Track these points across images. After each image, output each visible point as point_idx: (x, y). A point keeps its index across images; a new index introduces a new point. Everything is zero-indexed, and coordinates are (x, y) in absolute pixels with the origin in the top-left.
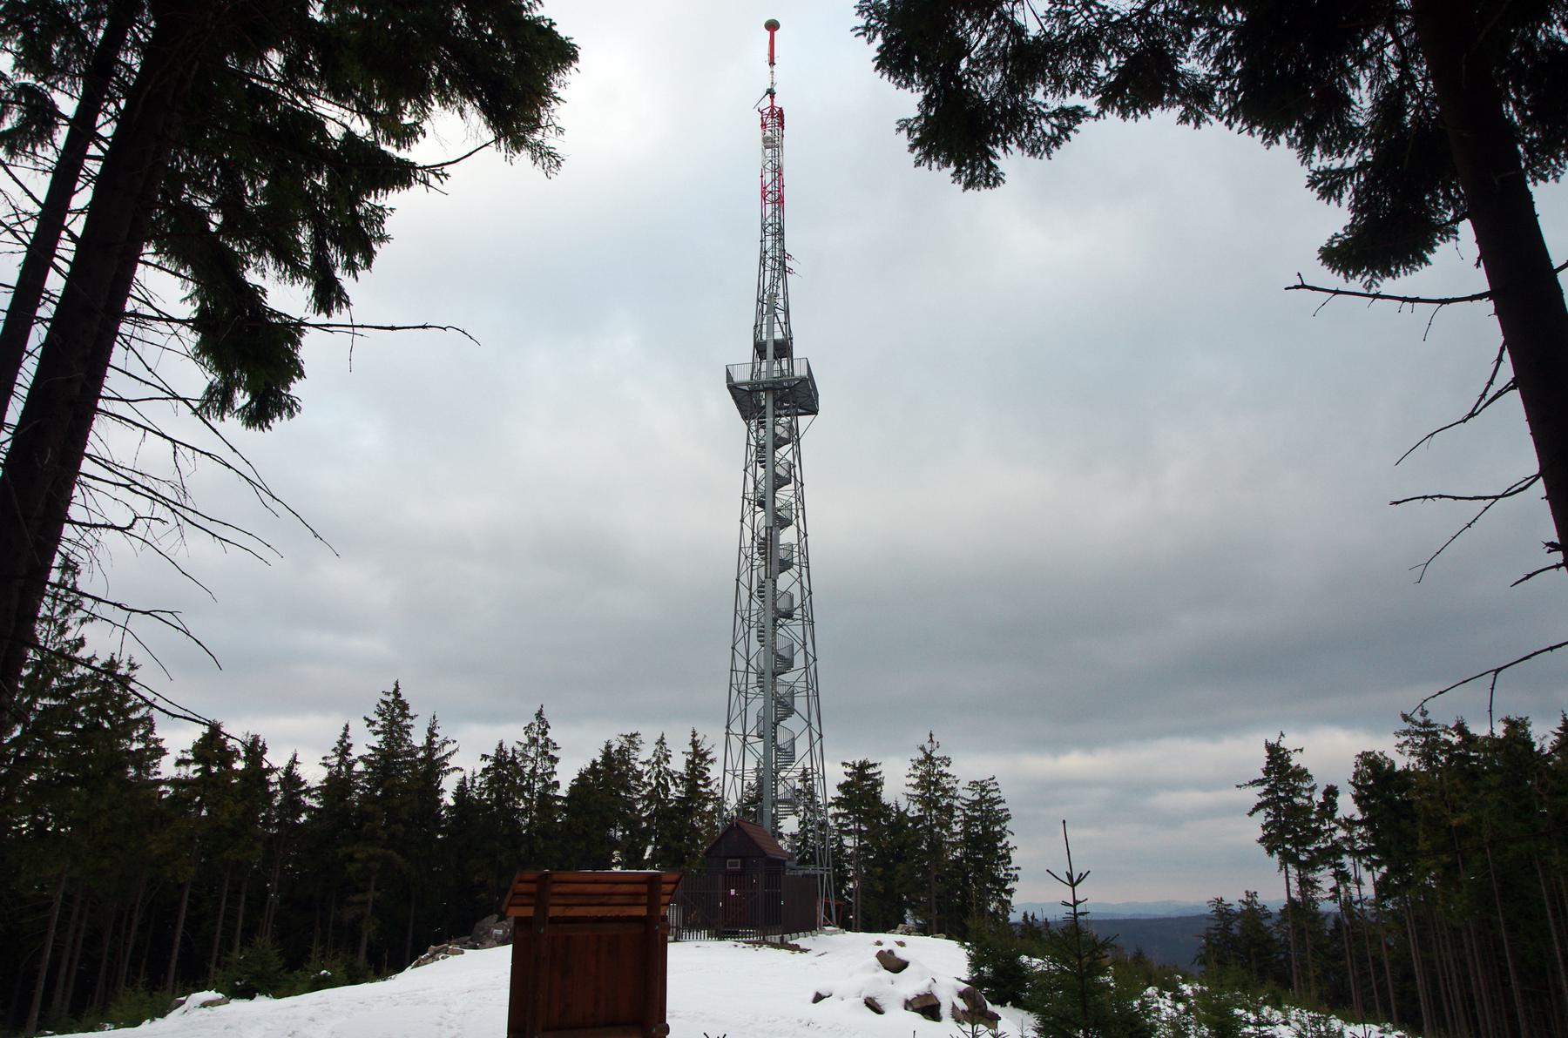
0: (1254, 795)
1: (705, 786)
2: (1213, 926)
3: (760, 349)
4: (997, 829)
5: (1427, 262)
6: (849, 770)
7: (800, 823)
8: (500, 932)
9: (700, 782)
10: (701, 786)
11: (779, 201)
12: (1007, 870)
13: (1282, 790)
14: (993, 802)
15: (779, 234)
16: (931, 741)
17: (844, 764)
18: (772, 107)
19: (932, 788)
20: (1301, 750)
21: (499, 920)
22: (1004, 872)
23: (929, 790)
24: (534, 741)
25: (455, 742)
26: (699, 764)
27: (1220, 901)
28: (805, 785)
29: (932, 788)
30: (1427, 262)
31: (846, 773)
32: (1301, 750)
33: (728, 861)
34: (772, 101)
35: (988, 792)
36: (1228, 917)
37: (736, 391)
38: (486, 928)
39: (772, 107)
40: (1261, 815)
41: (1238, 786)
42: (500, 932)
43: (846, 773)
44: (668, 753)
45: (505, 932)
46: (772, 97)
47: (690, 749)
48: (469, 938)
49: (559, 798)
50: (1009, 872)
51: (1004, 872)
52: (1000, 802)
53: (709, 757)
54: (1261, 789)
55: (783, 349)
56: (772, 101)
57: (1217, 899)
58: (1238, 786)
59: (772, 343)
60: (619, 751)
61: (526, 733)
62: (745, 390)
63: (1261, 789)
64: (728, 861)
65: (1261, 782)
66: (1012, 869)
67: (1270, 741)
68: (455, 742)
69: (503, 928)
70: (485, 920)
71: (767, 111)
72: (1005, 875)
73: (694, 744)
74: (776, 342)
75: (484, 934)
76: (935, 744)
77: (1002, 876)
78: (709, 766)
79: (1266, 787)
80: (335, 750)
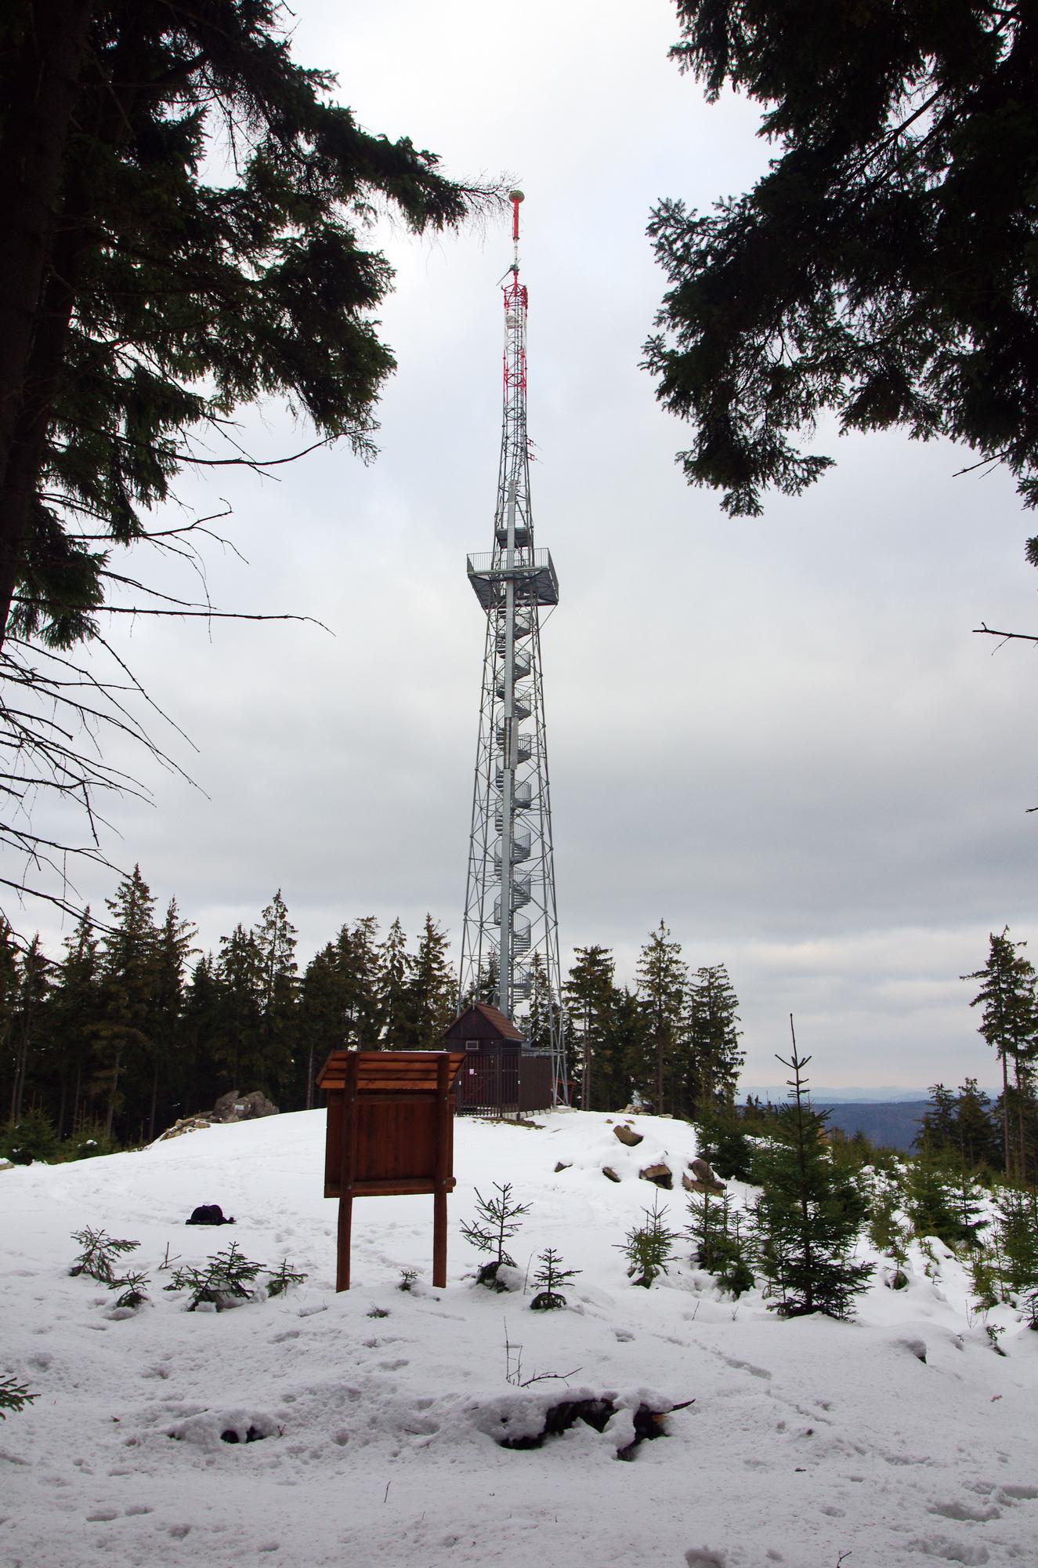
0: (978, 986)
1: (439, 969)
4: (725, 1014)
6: (581, 955)
7: (531, 1006)
8: (242, 1107)
9: (435, 965)
11: (522, 384)
12: (733, 1054)
13: (1004, 982)
15: (522, 418)
19: (662, 974)
20: (1025, 944)
21: (240, 1096)
23: (659, 976)
25: (194, 924)
28: (537, 970)
29: (662, 974)
31: (578, 959)
32: (1025, 944)
34: (516, 278)
35: (717, 979)
40: (984, 1003)
42: (242, 1107)
43: (578, 959)
44: (403, 937)
45: (246, 1107)
46: (516, 274)
47: (426, 934)
48: (211, 1113)
50: (735, 1056)
52: (728, 988)
53: (443, 941)
54: (985, 980)
55: (524, 538)
59: (513, 532)
61: (264, 916)
63: (985, 980)
65: (985, 974)
67: (995, 935)
68: (194, 924)
71: (510, 289)
72: (731, 1059)
73: (429, 928)
74: (517, 531)
77: (728, 1060)
79: (989, 978)
80: (76, 931)
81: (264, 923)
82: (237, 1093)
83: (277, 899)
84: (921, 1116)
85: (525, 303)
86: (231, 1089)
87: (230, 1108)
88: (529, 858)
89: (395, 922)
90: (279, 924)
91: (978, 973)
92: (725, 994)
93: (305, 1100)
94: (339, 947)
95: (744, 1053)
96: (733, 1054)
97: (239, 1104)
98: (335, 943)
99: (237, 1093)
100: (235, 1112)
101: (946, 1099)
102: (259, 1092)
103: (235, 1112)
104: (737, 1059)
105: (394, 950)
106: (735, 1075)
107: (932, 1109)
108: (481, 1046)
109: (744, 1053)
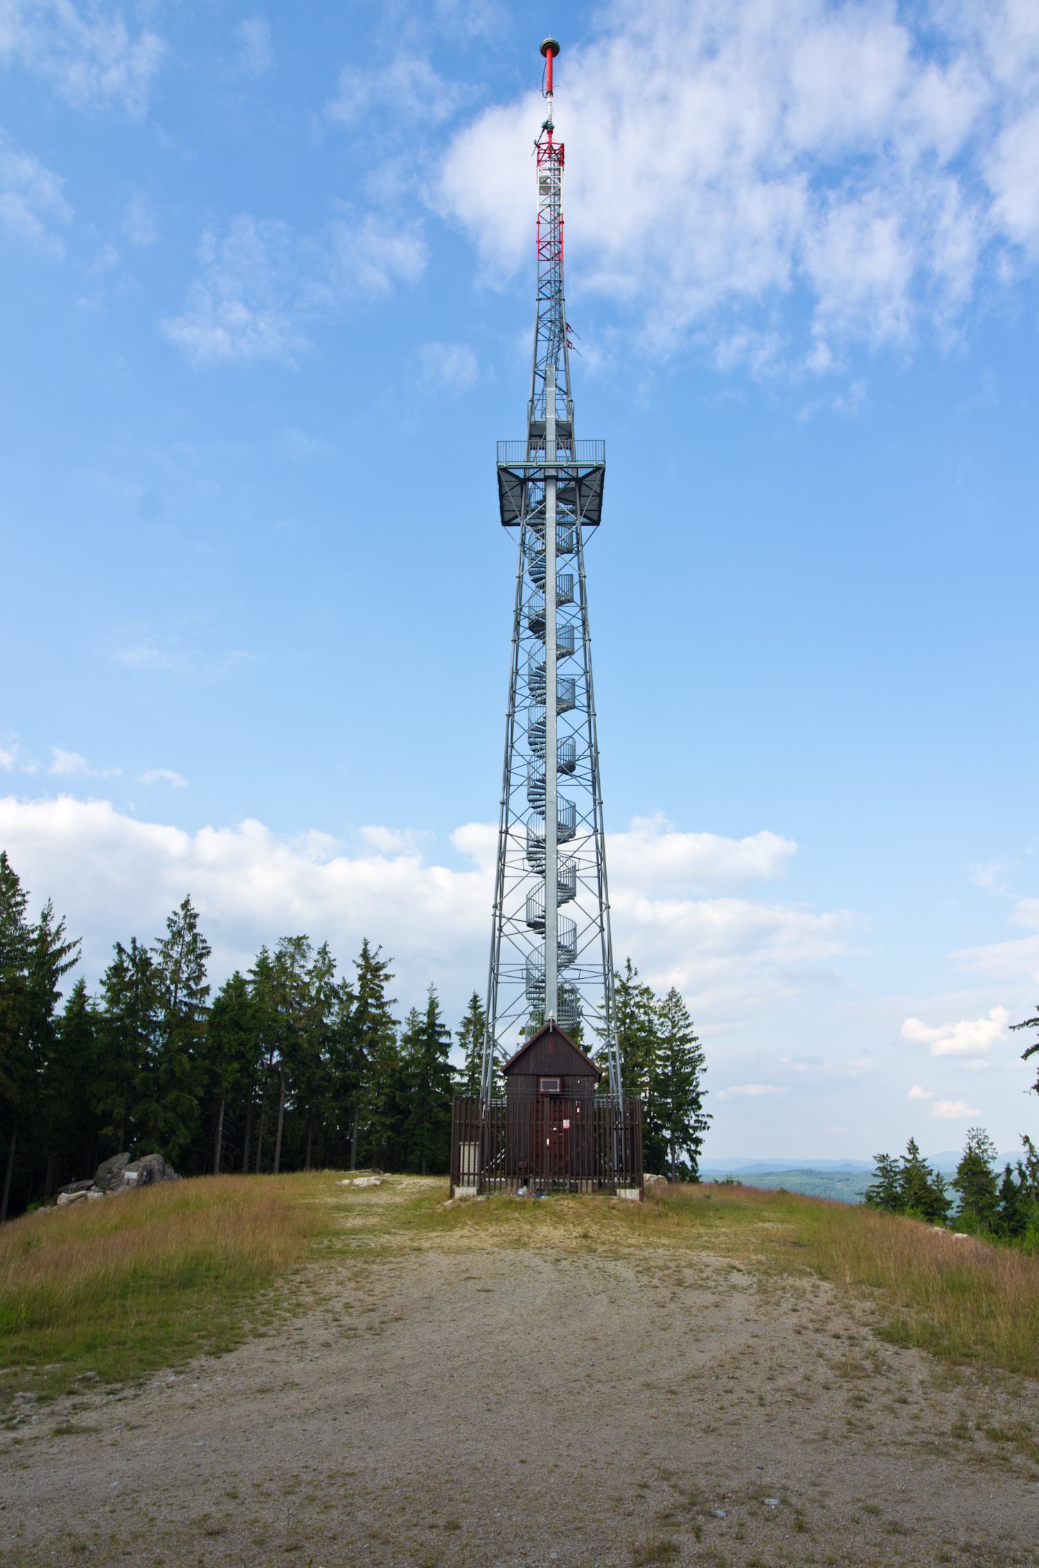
2: (877, 1184)
3: (536, 434)
5: (68, 1001)
7: (468, 1056)
10: (372, 1005)
12: (697, 1116)
14: (685, 1039)
16: (629, 967)
18: (550, 143)
19: (628, 1021)
21: (131, 1160)
22: (694, 1118)
23: (624, 1023)
24: (177, 935)
26: (371, 981)
27: (883, 1158)
29: (628, 1021)
30: (68, 1001)
33: (542, 1080)
35: (680, 1029)
36: (892, 1174)
37: (505, 477)
38: (115, 1170)
39: (550, 143)
41: (1011, 1027)
45: (141, 1175)
46: (550, 132)
48: (91, 1182)
49: (205, 1010)
50: (700, 1118)
51: (694, 1118)
52: (690, 1040)
56: (550, 137)
57: (883, 1156)
58: (1011, 1027)
59: (554, 423)
60: (279, 957)
62: (517, 477)
64: (542, 1080)
66: (703, 1115)
69: (137, 1170)
70: (113, 1159)
71: (544, 147)
72: (696, 1121)
75: (113, 1177)
76: (633, 972)
77: (692, 1122)
78: (384, 984)
81: (167, 936)
83: (185, 905)
84: (865, 1188)
85: (561, 162)
86: (114, 1152)
87: (118, 1176)
88: (575, 838)
89: (322, 946)
90: (188, 938)
91: (1030, 1021)
92: (687, 1046)
93: (304, 1161)
94: (233, 980)
95: (711, 1116)
96: (697, 1116)
98: (231, 978)
99: (127, 1155)
100: (125, 1182)
101: (891, 1171)
102: (154, 1155)
103: (125, 1182)
104: (701, 1122)
105: (320, 981)
106: (698, 1141)
107: (877, 1181)
108: (563, 1085)
109: (711, 1116)
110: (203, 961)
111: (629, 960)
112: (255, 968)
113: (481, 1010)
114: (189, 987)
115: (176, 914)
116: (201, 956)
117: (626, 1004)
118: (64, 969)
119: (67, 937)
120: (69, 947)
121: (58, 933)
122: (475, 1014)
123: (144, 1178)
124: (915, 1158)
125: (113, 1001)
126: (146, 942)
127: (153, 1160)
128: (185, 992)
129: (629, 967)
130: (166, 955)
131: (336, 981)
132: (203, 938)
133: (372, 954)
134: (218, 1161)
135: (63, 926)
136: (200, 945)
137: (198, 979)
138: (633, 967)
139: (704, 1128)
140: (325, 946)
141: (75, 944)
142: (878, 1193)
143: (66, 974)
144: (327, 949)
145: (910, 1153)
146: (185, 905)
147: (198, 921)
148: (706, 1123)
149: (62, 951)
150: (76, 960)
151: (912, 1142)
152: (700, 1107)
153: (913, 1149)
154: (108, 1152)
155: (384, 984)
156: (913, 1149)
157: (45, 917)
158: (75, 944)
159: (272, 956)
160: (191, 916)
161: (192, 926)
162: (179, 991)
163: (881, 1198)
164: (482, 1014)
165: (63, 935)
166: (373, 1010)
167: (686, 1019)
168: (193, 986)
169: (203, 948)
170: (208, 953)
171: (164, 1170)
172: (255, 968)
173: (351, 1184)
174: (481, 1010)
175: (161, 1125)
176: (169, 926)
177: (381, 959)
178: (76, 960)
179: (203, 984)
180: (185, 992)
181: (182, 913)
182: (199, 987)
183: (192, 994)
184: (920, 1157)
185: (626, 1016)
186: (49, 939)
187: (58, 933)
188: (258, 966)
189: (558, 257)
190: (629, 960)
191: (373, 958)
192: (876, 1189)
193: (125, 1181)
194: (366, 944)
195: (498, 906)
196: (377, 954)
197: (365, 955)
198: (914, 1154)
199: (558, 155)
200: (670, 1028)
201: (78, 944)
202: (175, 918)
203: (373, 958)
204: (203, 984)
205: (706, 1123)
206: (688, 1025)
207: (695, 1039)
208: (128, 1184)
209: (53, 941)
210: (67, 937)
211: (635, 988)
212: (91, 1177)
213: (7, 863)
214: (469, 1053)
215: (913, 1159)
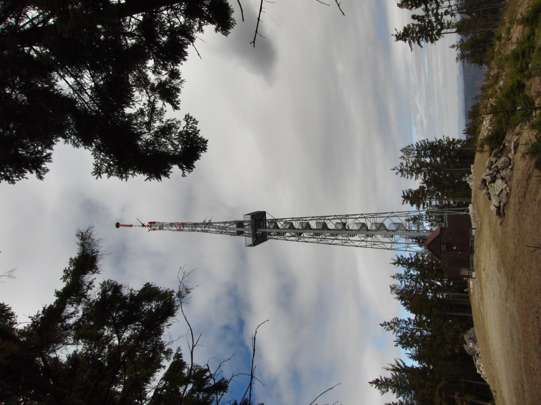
3: (240, 233)
6: (405, 202)
16: (394, 169)
17: (403, 204)
21: (466, 344)
24: (392, 328)
27: (457, 58)
33: (442, 250)
38: (469, 350)
45: (471, 342)
47: (397, 265)
54: (413, 43)
55: (240, 224)
60: (398, 294)
66: (444, 139)
70: (466, 350)
78: (404, 257)
81: (392, 331)
82: (464, 345)
83: (382, 325)
87: (471, 349)
89: (392, 277)
92: (420, 145)
95: (444, 136)
96: (444, 141)
97: (470, 345)
99: (464, 345)
102: (464, 337)
109: (444, 136)
110: (399, 320)
111: (391, 169)
112: (400, 301)
113: (410, 218)
114: (408, 324)
115: (385, 328)
116: (398, 321)
117: (407, 170)
118: (404, 364)
119: (394, 363)
120: (397, 362)
121: (393, 366)
122: (412, 220)
123: (472, 341)
124: (457, 46)
125: (411, 346)
126: (395, 338)
127: (466, 337)
128: (410, 325)
129: (394, 169)
130: (398, 331)
131: (403, 273)
132: (392, 320)
133: (394, 262)
134: (466, 315)
135: (391, 364)
136: (394, 321)
137: (406, 322)
138: (393, 168)
139: (449, 138)
140: (391, 276)
141: (396, 360)
142: (471, 60)
143: (405, 363)
144: (393, 276)
145: (454, 48)
146: (382, 325)
147: (387, 321)
148: (446, 138)
149: (398, 365)
150: (401, 360)
151: (451, 47)
152: (440, 140)
153: (453, 46)
154: (463, 350)
155: (404, 257)
156: (453, 46)
157: (388, 370)
158: (396, 360)
159: (397, 296)
160: (385, 324)
161: (389, 323)
162: (410, 327)
163: (472, 59)
164: (411, 218)
165: (393, 364)
166: (413, 261)
167: (410, 146)
168: (408, 323)
169: (395, 320)
170: (397, 318)
171: (469, 334)
172: (400, 301)
173: (472, 289)
174: (410, 218)
175: (453, 334)
176: (388, 330)
177: (396, 259)
178: (401, 360)
179: (407, 320)
180: (410, 325)
181: (384, 326)
182: (408, 321)
183: (410, 323)
184: (456, 44)
185: (411, 170)
186: (394, 368)
187: (393, 366)
188: (400, 300)
189: (183, 224)
190: (391, 169)
191: (395, 261)
192: (469, 61)
193: (473, 347)
194: (391, 263)
195: (388, 249)
196: (394, 260)
197: (395, 264)
198: (455, 46)
199: (152, 224)
200: (414, 152)
201: (396, 359)
202: (386, 328)
203: (395, 261)
204: (407, 320)
205: (446, 138)
206: (412, 145)
207: (417, 143)
208: (474, 346)
209: (395, 367)
210: (394, 363)
211: (401, 167)
212: (471, 357)
213: (372, 382)
214: (425, 222)
215: (457, 46)
